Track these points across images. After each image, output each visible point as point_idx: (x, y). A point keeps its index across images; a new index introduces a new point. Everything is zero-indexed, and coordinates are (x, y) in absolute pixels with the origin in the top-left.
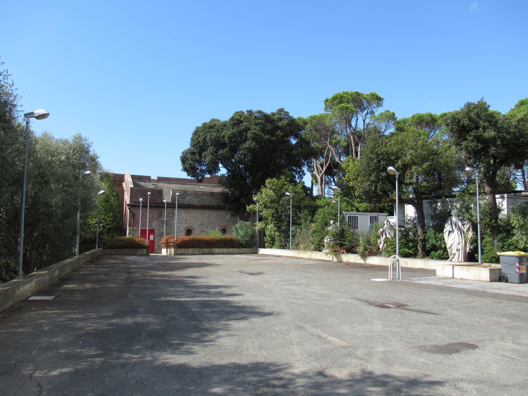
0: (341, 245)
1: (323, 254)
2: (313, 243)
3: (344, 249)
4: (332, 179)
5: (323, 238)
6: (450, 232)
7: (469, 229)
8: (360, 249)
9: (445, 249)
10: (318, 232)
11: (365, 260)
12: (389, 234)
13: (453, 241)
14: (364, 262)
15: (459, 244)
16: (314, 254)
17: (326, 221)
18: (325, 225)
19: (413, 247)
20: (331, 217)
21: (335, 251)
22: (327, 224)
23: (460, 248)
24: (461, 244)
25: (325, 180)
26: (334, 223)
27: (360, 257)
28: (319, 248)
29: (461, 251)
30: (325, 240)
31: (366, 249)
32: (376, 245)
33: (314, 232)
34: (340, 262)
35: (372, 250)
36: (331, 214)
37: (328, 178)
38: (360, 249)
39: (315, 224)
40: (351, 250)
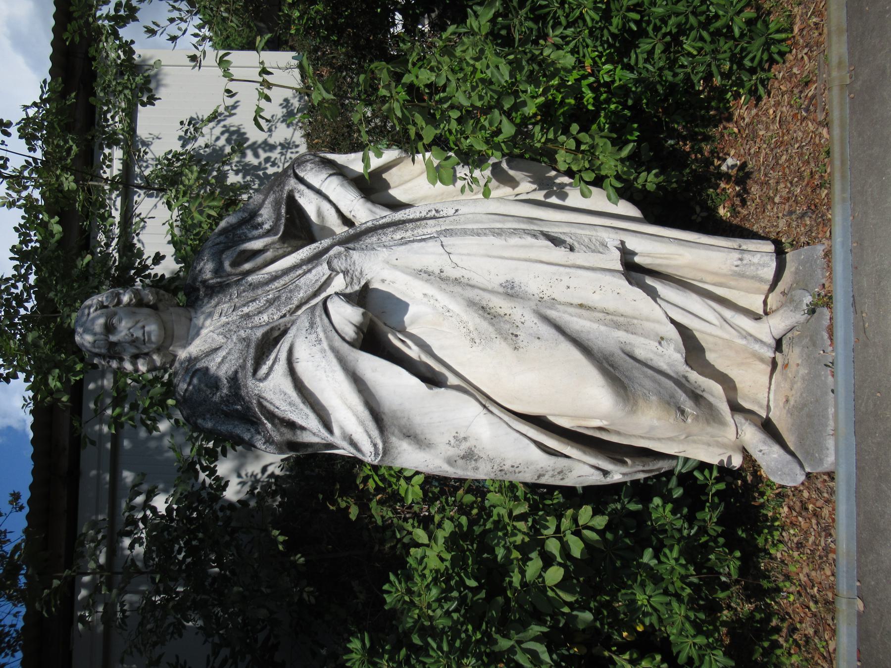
6: (372, 340)
7: (371, 187)
15: (556, 241)
24: (553, 230)
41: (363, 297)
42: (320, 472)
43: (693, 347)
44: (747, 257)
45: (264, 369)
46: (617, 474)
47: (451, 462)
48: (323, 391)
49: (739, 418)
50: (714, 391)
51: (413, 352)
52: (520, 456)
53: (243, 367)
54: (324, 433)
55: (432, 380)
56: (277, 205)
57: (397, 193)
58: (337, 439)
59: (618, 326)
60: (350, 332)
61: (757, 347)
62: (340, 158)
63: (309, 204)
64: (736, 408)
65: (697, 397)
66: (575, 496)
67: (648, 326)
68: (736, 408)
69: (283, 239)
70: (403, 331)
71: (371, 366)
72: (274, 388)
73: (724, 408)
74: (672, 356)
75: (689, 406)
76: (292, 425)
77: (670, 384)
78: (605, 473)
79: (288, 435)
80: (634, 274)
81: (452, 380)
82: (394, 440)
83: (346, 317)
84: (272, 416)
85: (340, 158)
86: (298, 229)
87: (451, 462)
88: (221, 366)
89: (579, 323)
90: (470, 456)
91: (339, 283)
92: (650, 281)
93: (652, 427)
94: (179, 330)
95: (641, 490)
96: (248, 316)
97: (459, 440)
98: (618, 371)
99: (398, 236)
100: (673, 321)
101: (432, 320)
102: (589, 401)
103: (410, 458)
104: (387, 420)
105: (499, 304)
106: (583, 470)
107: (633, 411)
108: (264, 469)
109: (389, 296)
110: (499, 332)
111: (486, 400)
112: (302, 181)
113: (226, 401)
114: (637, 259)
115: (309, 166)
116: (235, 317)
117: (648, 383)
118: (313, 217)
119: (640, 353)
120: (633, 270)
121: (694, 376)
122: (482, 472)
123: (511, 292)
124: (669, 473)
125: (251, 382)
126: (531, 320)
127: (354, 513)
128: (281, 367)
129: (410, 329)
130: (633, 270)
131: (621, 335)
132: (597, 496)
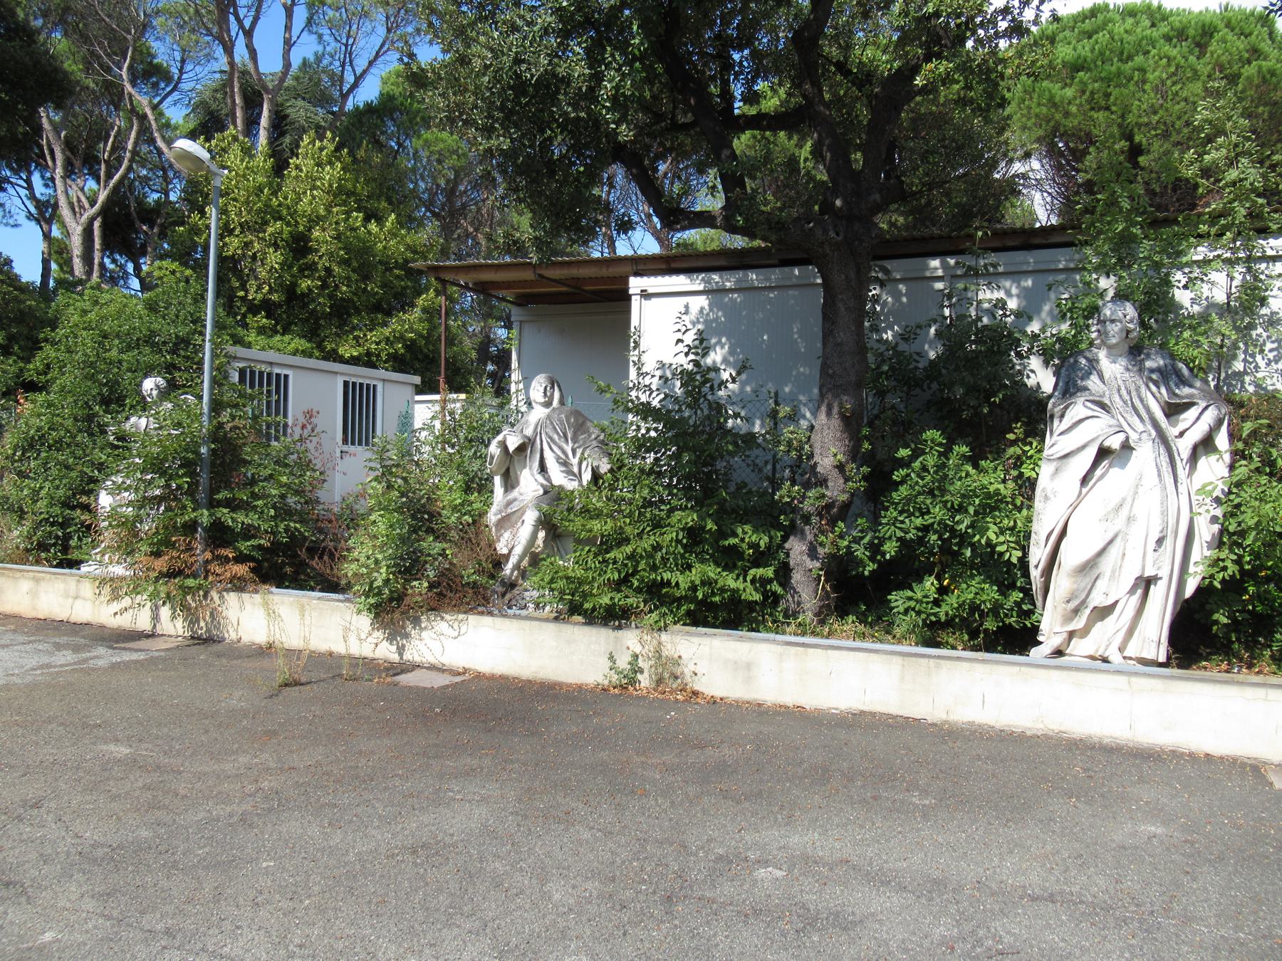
0: (219, 536)
1: (88, 589)
2: (21, 514)
3: (241, 559)
4: (130, 267)
5: (89, 486)
6: (1103, 453)
7: (1206, 445)
8: (367, 554)
9: (1009, 574)
10: (58, 445)
11: (396, 633)
12: (565, 464)
13: (1119, 523)
14: (388, 652)
15: (1160, 542)
16: (25, 585)
17: (113, 385)
18: (106, 402)
19: (760, 558)
20: (147, 355)
21: (171, 574)
22: (117, 398)
23: (1164, 573)
24: (1168, 542)
25: (102, 265)
26: (164, 394)
27: (365, 621)
28: (59, 546)
29: (1157, 592)
30: (105, 500)
31: (409, 567)
32: (473, 532)
33: (30, 445)
34: (206, 641)
35: (439, 568)
36: (149, 340)
37: (114, 261)
38: (367, 554)
39: (41, 397)
40: (297, 560)
41: (1127, 447)
42: (1034, 416)
43: (1104, 612)
44: (1154, 645)
45: (1089, 404)
46: (1035, 574)
47: (1044, 490)
48: (1075, 432)
49: (1065, 635)
50: (1079, 623)
51: (1098, 472)
52: (1045, 518)
53: (1091, 394)
54: (1058, 432)
55: (1085, 481)
56: (1192, 396)
57: (1203, 462)
58: (1055, 437)
59: (1113, 572)
60: (1106, 444)
61: (1103, 647)
62: (1224, 428)
63: (1192, 413)
64: (1071, 634)
65: (1076, 611)
66: (1025, 550)
67: (1113, 586)
68: (1071, 634)
69: (1167, 403)
70: (1110, 466)
71: (1091, 452)
72: (1078, 409)
73: (1071, 627)
74: (1097, 599)
75: (1072, 605)
76: (1062, 416)
77: (1083, 596)
78: (1036, 567)
79: (1057, 415)
80: (1143, 584)
81: (1084, 490)
82: (1055, 464)
83: (1115, 442)
84: (1066, 408)
85: (1224, 428)
86: (1174, 410)
87: (1044, 490)
88: (1093, 382)
89: (1114, 551)
90: (1046, 498)
91: (1133, 436)
92: (1139, 592)
93: (1062, 584)
94: (1114, 351)
95: (1027, 591)
96: (1119, 390)
97: (1055, 494)
98: (1089, 567)
99: (1164, 464)
100: (1117, 602)
101: (1114, 480)
102: (1072, 555)
103: (1045, 471)
104: (1065, 461)
105: (1124, 512)
106: (1038, 555)
107: (1069, 575)
108: (1033, 371)
109: (1128, 460)
110: (1109, 513)
111: (1074, 507)
112: (1206, 408)
113: (1075, 385)
114: (1152, 587)
115: (1216, 412)
116: (1120, 382)
117: (1083, 585)
118: (1182, 417)
119: (1099, 583)
120: (1146, 583)
121: (1088, 611)
122: (1038, 503)
123: (1130, 519)
124: (1034, 605)
125: (1082, 399)
126: (1116, 529)
127: (1011, 436)
128: (1090, 413)
129: (1111, 470)
130: (1146, 583)
131: (1108, 574)
132: (1024, 564)
